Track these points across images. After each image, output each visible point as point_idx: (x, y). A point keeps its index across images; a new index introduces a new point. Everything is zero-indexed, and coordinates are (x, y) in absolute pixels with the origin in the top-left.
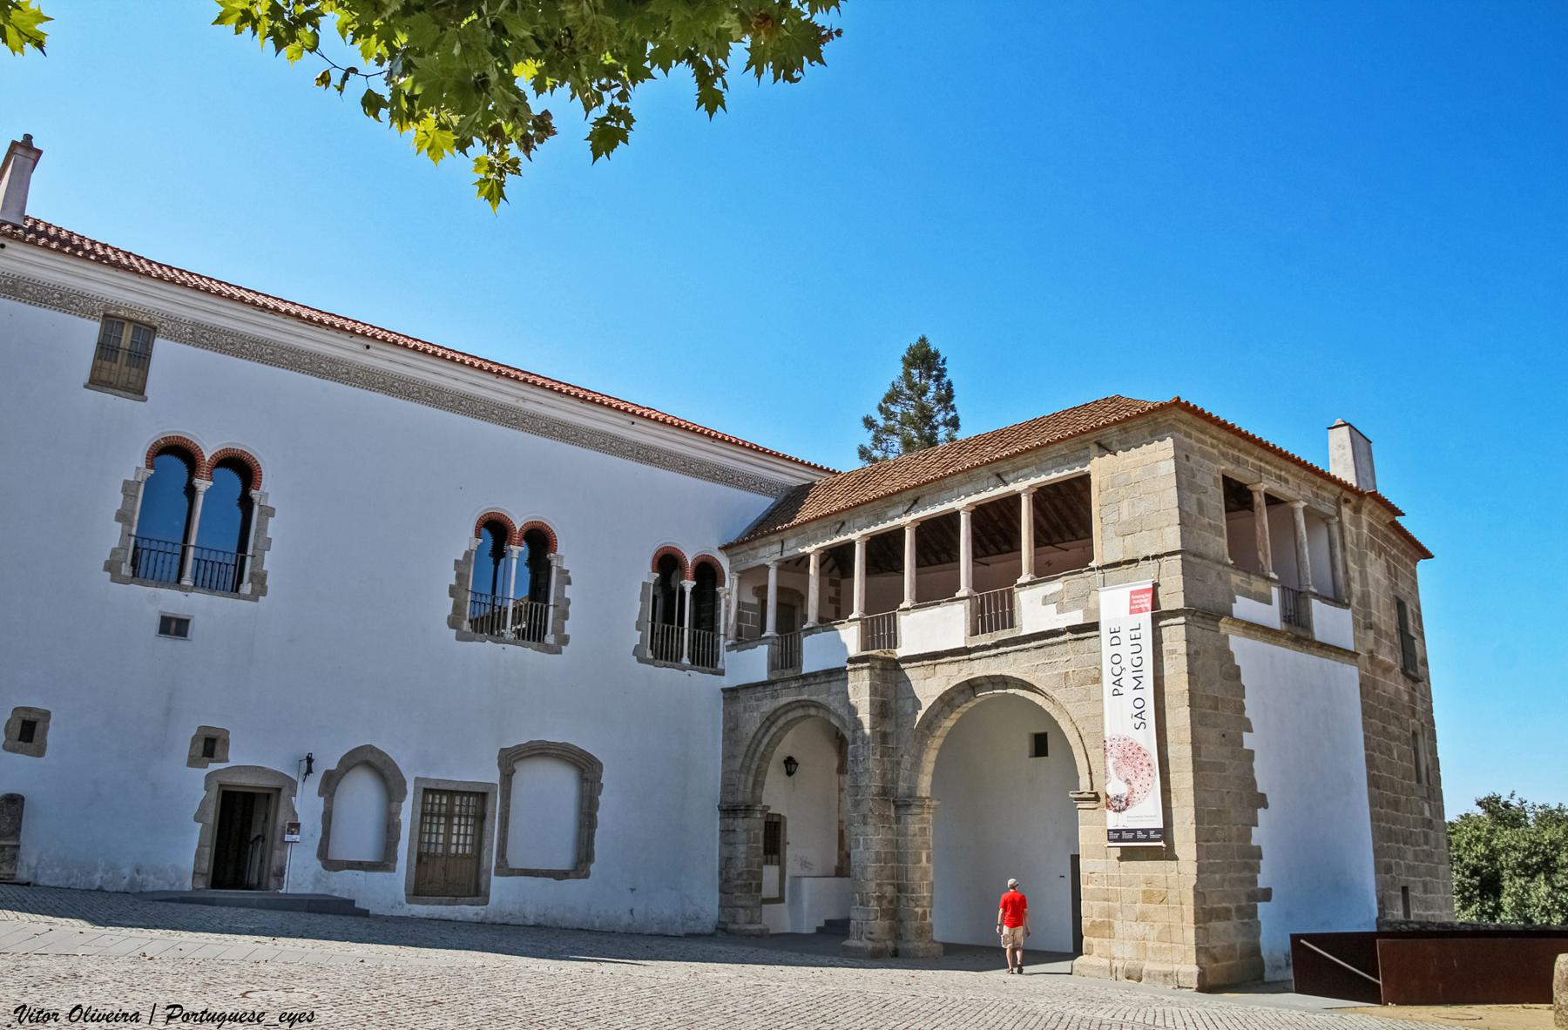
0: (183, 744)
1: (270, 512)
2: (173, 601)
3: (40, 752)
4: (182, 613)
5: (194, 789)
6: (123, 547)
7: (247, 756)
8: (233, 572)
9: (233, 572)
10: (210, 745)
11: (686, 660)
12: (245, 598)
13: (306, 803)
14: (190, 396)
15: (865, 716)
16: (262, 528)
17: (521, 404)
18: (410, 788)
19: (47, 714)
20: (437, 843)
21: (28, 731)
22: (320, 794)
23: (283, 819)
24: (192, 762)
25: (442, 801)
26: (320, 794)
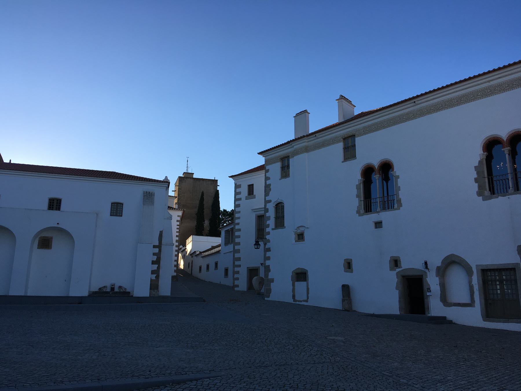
0: (387, 265)
1: (398, 177)
2: (374, 217)
3: (352, 272)
4: (379, 220)
5: (392, 278)
6: (360, 205)
7: (411, 263)
8: (390, 202)
9: (390, 202)
10: (396, 262)
11: (511, 190)
12: (396, 209)
13: (432, 281)
14: (371, 150)
15: (188, 253)
16: (397, 184)
17: (492, 83)
18: (474, 270)
19: (351, 260)
20: (497, 294)
21: (349, 265)
22: (437, 276)
23: (425, 288)
24: (392, 269)
25: (488, 274)
26: (437, 276)
